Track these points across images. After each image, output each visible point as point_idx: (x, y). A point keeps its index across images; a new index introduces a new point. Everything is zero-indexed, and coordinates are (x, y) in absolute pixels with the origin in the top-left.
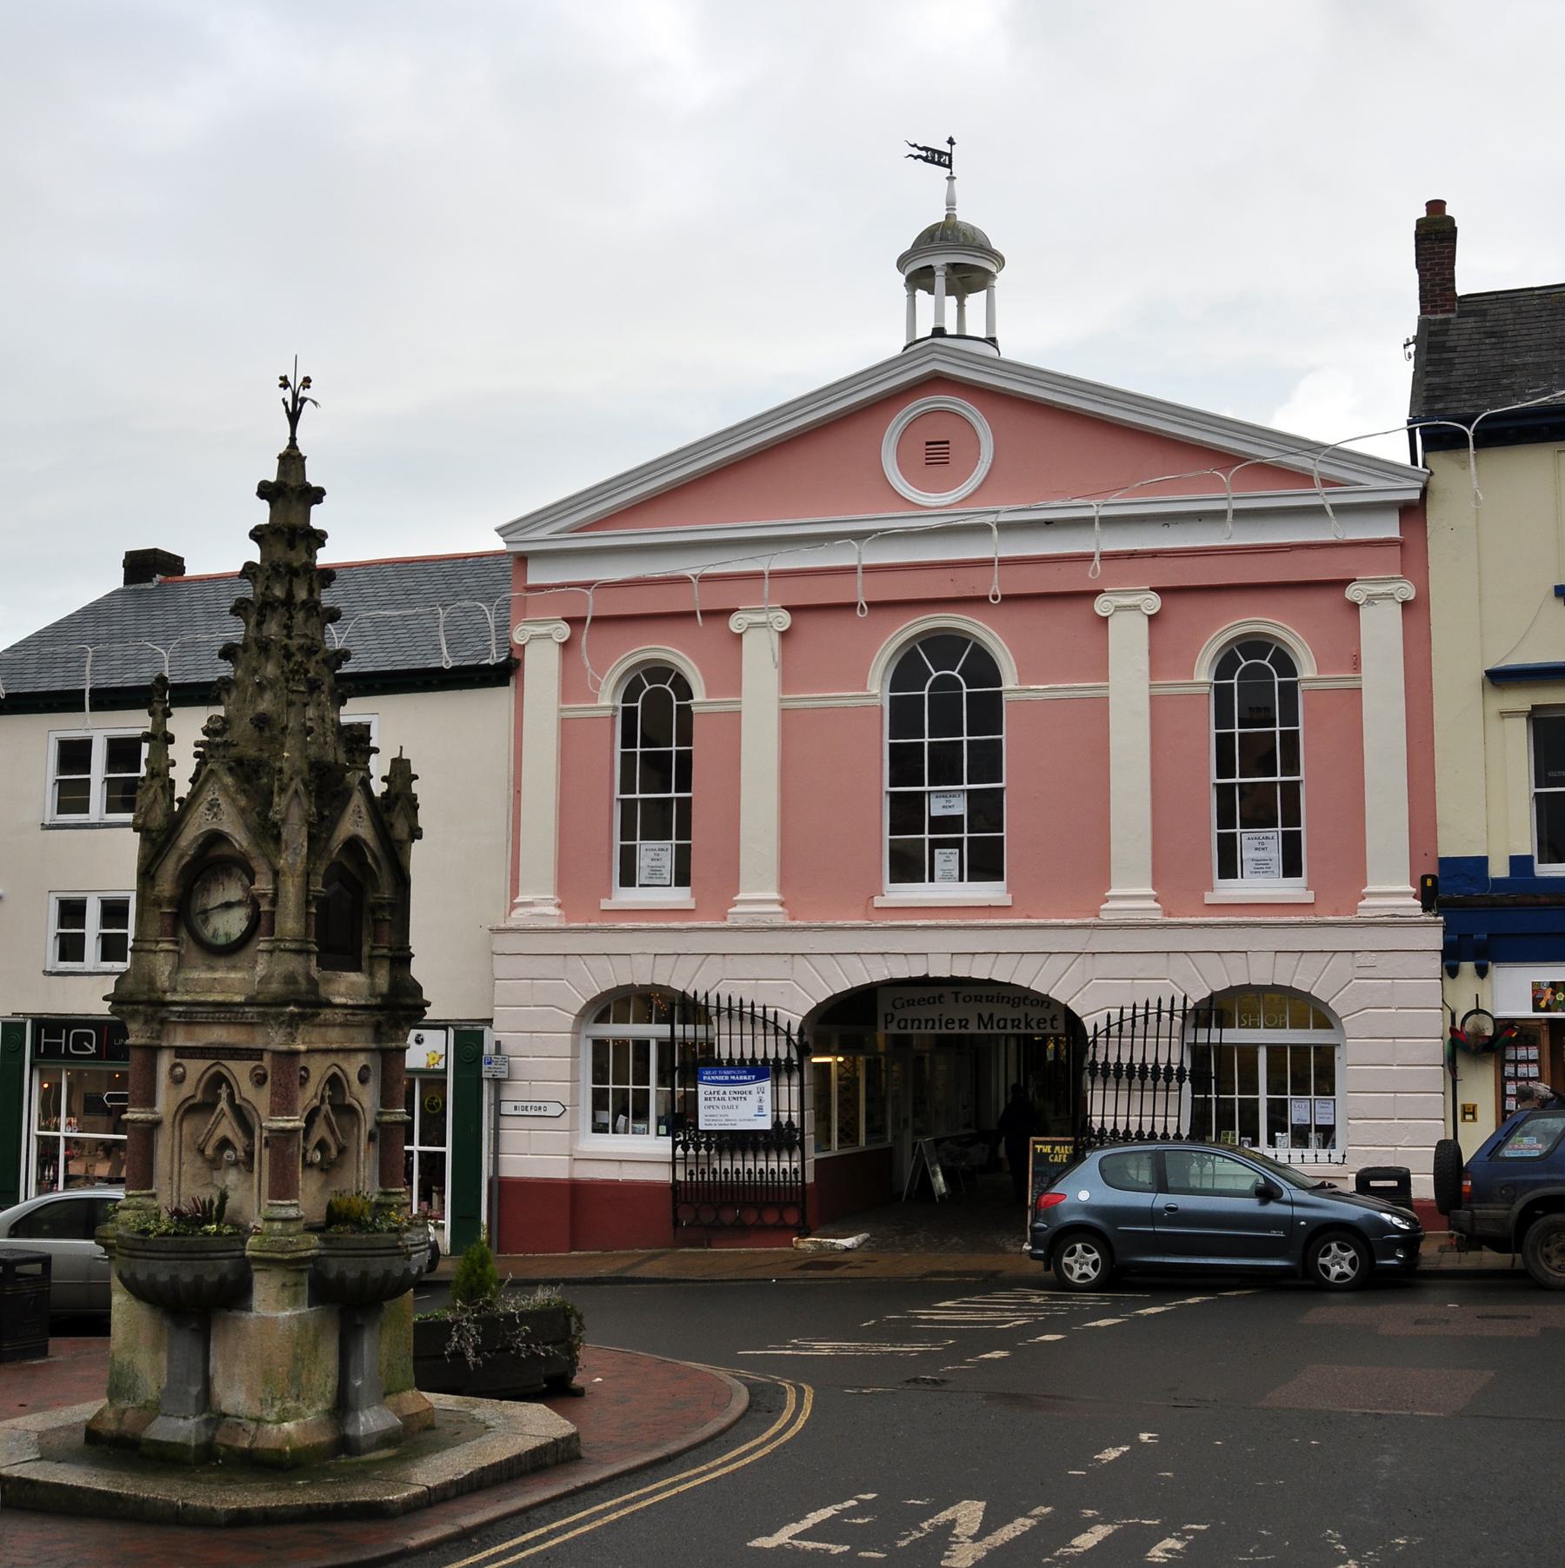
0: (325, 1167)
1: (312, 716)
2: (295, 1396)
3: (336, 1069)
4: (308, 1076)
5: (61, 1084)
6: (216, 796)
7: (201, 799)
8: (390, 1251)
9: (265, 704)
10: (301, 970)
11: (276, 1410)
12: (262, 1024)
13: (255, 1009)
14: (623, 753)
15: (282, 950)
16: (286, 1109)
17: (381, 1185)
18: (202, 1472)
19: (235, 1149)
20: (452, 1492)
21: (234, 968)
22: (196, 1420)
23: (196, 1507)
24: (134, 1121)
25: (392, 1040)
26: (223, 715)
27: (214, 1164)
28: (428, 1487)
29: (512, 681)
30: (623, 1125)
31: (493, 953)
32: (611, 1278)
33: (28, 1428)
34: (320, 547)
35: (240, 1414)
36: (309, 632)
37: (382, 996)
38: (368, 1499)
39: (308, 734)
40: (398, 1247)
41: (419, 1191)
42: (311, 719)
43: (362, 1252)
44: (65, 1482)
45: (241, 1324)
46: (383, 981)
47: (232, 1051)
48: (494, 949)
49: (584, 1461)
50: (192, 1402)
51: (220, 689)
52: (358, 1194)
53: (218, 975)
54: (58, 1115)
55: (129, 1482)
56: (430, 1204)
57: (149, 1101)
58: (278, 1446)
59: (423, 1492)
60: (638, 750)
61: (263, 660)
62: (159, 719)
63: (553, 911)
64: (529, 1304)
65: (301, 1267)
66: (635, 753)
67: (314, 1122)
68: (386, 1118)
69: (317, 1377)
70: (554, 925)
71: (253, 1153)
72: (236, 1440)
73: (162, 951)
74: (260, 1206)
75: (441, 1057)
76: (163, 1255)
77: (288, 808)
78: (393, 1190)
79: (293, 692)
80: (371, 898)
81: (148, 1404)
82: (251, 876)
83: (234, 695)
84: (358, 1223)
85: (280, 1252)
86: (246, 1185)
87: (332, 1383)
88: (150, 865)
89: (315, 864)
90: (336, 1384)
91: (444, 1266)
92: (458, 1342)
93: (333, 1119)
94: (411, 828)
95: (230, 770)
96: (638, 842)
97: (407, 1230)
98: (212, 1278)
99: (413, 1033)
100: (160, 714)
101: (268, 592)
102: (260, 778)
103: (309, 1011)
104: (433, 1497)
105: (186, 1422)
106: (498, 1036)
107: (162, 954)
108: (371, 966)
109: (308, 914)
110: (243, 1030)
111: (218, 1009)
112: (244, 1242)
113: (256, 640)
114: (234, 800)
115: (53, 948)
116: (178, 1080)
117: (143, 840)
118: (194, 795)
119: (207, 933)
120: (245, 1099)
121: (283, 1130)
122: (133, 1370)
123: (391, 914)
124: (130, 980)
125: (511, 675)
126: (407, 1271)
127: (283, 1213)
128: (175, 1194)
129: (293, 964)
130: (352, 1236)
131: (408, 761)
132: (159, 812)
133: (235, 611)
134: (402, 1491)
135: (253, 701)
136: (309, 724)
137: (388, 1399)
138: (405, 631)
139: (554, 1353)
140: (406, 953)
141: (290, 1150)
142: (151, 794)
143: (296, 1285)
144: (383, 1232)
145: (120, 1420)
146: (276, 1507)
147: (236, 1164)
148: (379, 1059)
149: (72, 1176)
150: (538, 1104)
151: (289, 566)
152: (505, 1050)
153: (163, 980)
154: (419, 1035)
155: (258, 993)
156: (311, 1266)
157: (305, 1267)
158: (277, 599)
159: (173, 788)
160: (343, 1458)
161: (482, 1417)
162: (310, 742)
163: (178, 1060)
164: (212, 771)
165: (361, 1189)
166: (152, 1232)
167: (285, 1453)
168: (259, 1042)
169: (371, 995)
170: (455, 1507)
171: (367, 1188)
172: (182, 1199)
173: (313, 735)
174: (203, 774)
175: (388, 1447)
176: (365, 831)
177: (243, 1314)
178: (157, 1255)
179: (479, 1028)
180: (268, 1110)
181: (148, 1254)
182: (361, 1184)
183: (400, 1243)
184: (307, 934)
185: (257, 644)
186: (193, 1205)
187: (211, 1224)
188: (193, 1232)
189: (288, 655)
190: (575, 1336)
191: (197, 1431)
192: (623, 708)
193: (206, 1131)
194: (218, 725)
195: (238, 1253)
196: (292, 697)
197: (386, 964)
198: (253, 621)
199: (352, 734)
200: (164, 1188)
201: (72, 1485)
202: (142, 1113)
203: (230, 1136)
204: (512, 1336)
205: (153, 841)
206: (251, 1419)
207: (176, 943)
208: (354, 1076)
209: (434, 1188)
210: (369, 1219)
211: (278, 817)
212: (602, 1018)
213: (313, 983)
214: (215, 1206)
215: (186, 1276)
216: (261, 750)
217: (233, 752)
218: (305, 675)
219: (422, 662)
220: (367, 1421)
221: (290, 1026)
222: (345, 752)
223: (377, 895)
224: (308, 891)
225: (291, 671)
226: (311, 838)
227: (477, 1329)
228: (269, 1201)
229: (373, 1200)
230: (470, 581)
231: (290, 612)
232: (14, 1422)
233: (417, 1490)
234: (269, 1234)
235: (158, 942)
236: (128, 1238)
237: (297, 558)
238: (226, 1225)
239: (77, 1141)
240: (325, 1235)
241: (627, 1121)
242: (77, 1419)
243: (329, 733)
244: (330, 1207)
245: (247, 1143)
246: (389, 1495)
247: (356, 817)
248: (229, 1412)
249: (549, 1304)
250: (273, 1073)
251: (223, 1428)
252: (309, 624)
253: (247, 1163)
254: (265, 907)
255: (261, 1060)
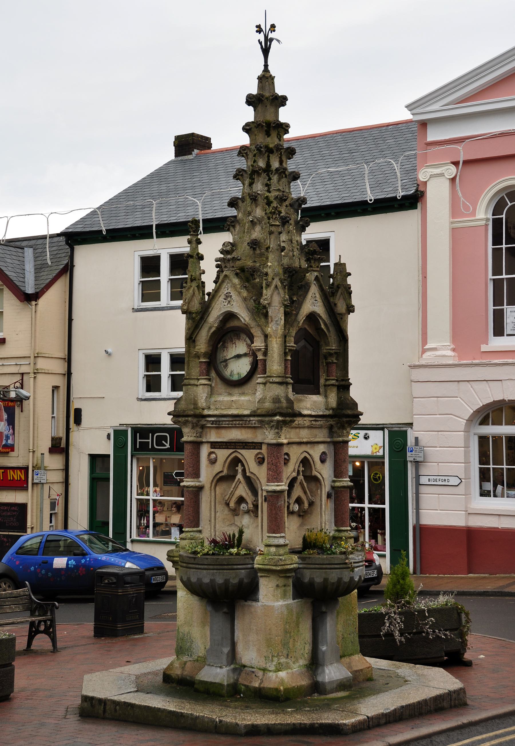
0: (301, 514)
1: (284, 240)
2: (285, 655)
3: (306, 454)
4: (289, 459)
5: (150, 467)
6: (229, 291)
7: (221, 293)
8: (341, 566)
9: (256, 234)
10: (283, 395)
11: (274, 663)
12: (260, 427)
13: (256, 419)
14: (493, 249)
15: (271, 383)
16: (276, 478)
17: (335, 525)
18: (231, 701)
19: (247, 503)
20: (383, 721)
21: (243, 394)
22: (228, 668)
23: (227, 723)
24: (187, 487)
25: (340, 436)
26: (232, 241)
27: (235, 512)
28: (367, 716)
29: (419, 205)
30: (500, 492)
31: (412, 381)
32: (495, 592)
33: (130, 673)
34: (286, 134)
35: (253, 666)
36: (281, 188)
37: (333, 409)
38: (330, 722)
39: (282, 251)
40: (346, 563)
41: (369, 533)
42: (284, 242)
43: (324, 566)
44: (151, 705)
45: (253, 610)
46: (333, 399)
47: (244, 444)
48: (412, 378)
49: (469, 707)
50: (224, 657)
51: (229, 225)
52: (321, 530)
53: (234, 398)
54: (148, 486)
55: (188, 706)
56: (377, 541)
57: (196, 475)
58: (276, 686)
59: (364, 719)
60: (504, 246)
61: (254, 207)
62: (194, 245)
63: (450, 353)
64: (434, 604)
65: (288, 575)
66: (502, 248)
67: (293, 486)
68: (337, 484)
69: (299, 644)
70: (451, 362)
71: (258, 506)
72: (251, 682)
73: (201, 385)
74: (262, 537)
75: (380, 447)
76: (206, 567)
77: (271, 297)
78: (343, 528)
79: (272, 225)
80: (324, 350)
81: (199, 659)
82: (251, 338)
83: (238, 228)
84: (322, 549)
85: (275, 565)
86: (254, 525)
87: (308, 648)
88: (192, 333)
89: (289, 330)
90: (310, 648)
91: (385, 581)
92: (389, 627)
93: (305, 484)
94: (347, 305)
95: (237, 274)
96: (505, 307)
97: (352, 553)
98: (235, 581)
99: (353, 432)
100: (194, 242)
101: (255, 164)
102: (255, 279)
103: (288, 419)
104: (371, 723)
105: (222, 670)
106: (417, 434)
107: (201, 387)
108: (326, 391)
109: (286, 360)
110: (249, 431)
111: (235, 419)
112: (253, 559)
113: (249, 194)
114: (239, 293)
115: (142, 384)
116: (213, 462)
117: (188, 319)
118: (216, 291)
119: (227, 373)
120: (252, 473)
121: (275, 492)
122: (190, 637)
123: (336, 359)
124: (183, 402)
125: (418, 202)
126: (352, 579)
127: (276, 542)
128: (212, 530)
129: (278, 391)
130: (318, 556)
131: (345, 264)
132: (196, 302)
133: (236, 177)
134: (351, 718)
135: (249, 232)
136: (283, 244)
137: (343, 659)
138: (349, 177)
139: (450, 636)
140: (347, 383)
141: (279, 503)
142: (191, 291)
143: (285, 586)
144: (337, 554)
145: (183, 668)
146: (275, 724)
147: (248, 512)
148: (332, 448)
149: (157, 523)
150: (444, 478)
151: (267, 147)
152: (422, 443)
153: (202, 402)
154: (366, 434)
155: (258, 409)
156: (294, 574)
157: (290, 575)
158: (261, 168)
159: (204, 287)
160: (316, 696)
161: (403, 675)
162: (284, 256)
163: (213, 450)
164: (226, 276)
165: (323, 527)
166: (199, 553)
167: (280, 691)
168: (259, 439)
169: (326, 409)
170: (384, 730)
171: (327, 527)
172: (217, 533)
173: (284, 251)
174: (221, 278)
175: (344, 690)
176: (319, 309)
177: (254, 603)
178: (202, 567)
179: (404, 429)
180: (266, 479)
181: (197, 566)
182: (323, 525)
183: (347, 561)
184: (286, 372)
185: (250, 197)
186: (223, 537)
187: (233, 548)
188: (223, 553)
189: (269, 203)
190: (465, 626)
191: (228, 676)
192: (493, 219)
193: (230, 492)
194: (228, 248)
195: (250, 566)
196: (273, 229)
197: (335, 389)
198: (247, 182)
199: (309, 250)
200: (206, 527)
201: (155, 707)
202: (192, 482)
203: (244, 495)
204: (423, 624)
205: (193, 319)
206: (260, 669)
207: (209, 380)
208: (317, 459)
209: (378, 531)
210: (328, 546)
211: (266, 302)
212: (484, 422)
213: (290, 402)
214: (236, 537)
215: (220, 580)
216: (255, 262)
217: (238, 263)
218: (279, 215)
219: (360, 196)
220: (330, 673)
221: (277, 428)
222: (305, 261)
223: (328, 348)
224: (286, 346)
225: (271, 213)
226: (286, 314)
227: (401, 619)
228: (268, 535)
229: (331, 535)
230: (391, 141)
231: (269, 176)
232: (122, 669)
233: (361, 718)
234: (268, 555)
235: (198, 379)
236: (186, 556)
237: (272, 141)
238: (242, 549)
239: (161, 503)
240: (301, 555)
241: (503, 489)
242: (158, 668)
243: (295, 250)
244: (304, 539)
245: (254, 499)
246: (343, 720)
247: (313, 300)
248: (246, 664)
249: (447, 605)
250: (268, 457)
251: (243, 675)
252: (281, 183)
253: (255, 511)
254: (260, 357)
255: (261, 449)
